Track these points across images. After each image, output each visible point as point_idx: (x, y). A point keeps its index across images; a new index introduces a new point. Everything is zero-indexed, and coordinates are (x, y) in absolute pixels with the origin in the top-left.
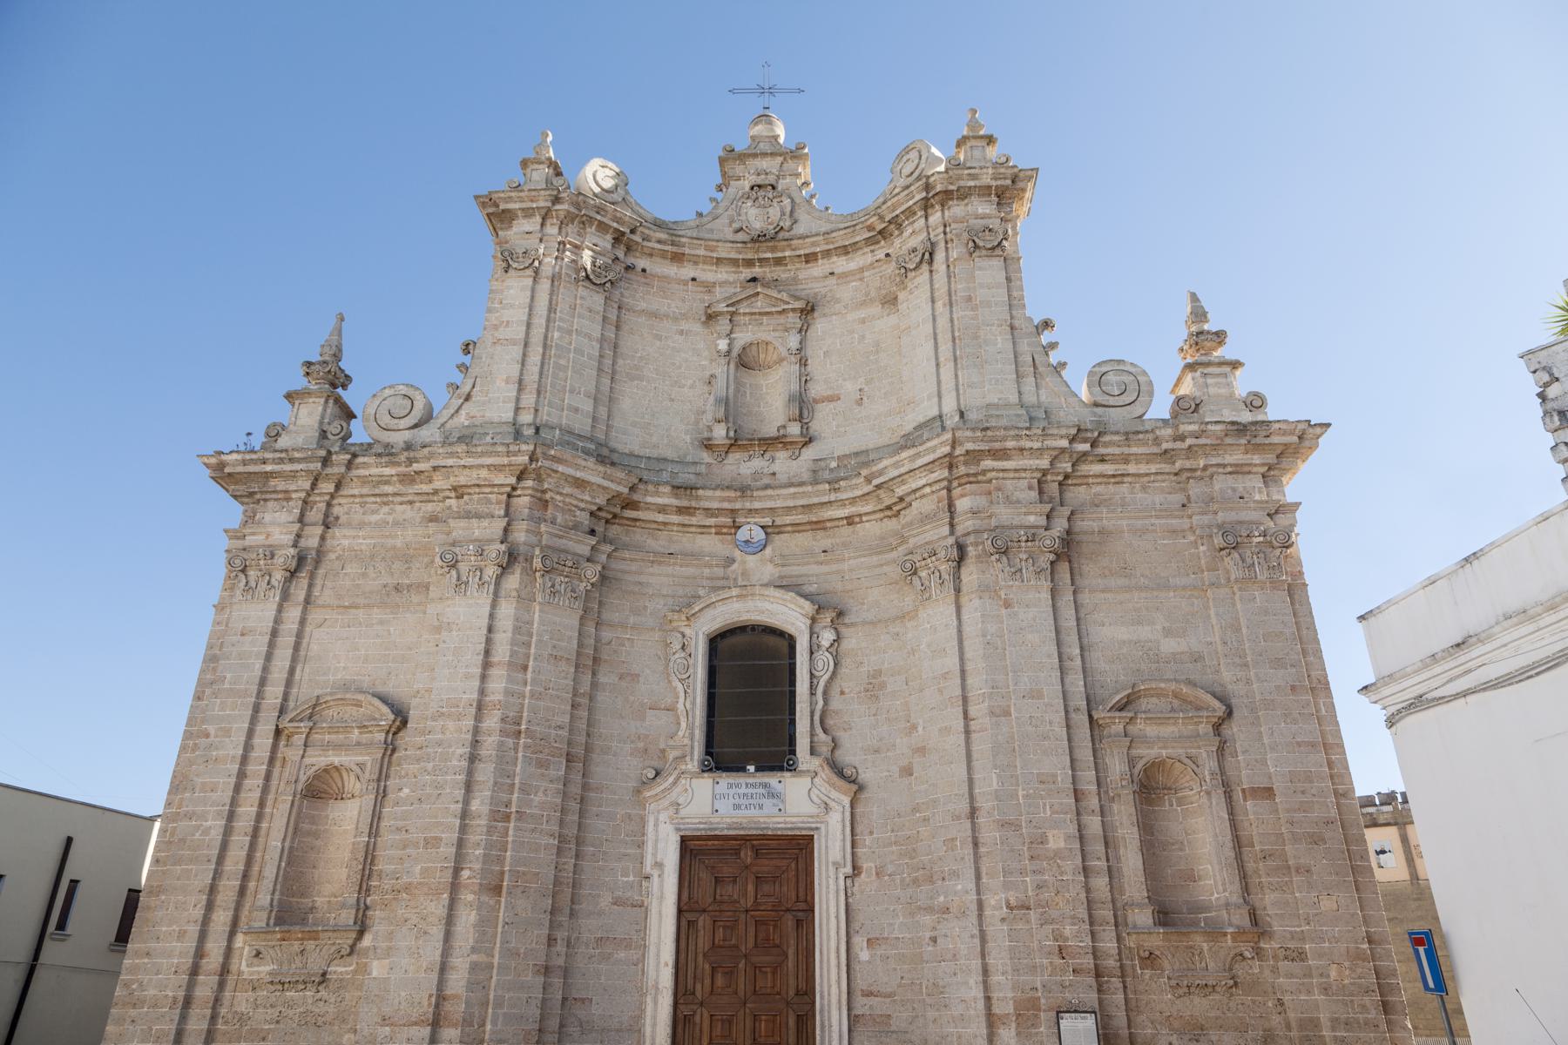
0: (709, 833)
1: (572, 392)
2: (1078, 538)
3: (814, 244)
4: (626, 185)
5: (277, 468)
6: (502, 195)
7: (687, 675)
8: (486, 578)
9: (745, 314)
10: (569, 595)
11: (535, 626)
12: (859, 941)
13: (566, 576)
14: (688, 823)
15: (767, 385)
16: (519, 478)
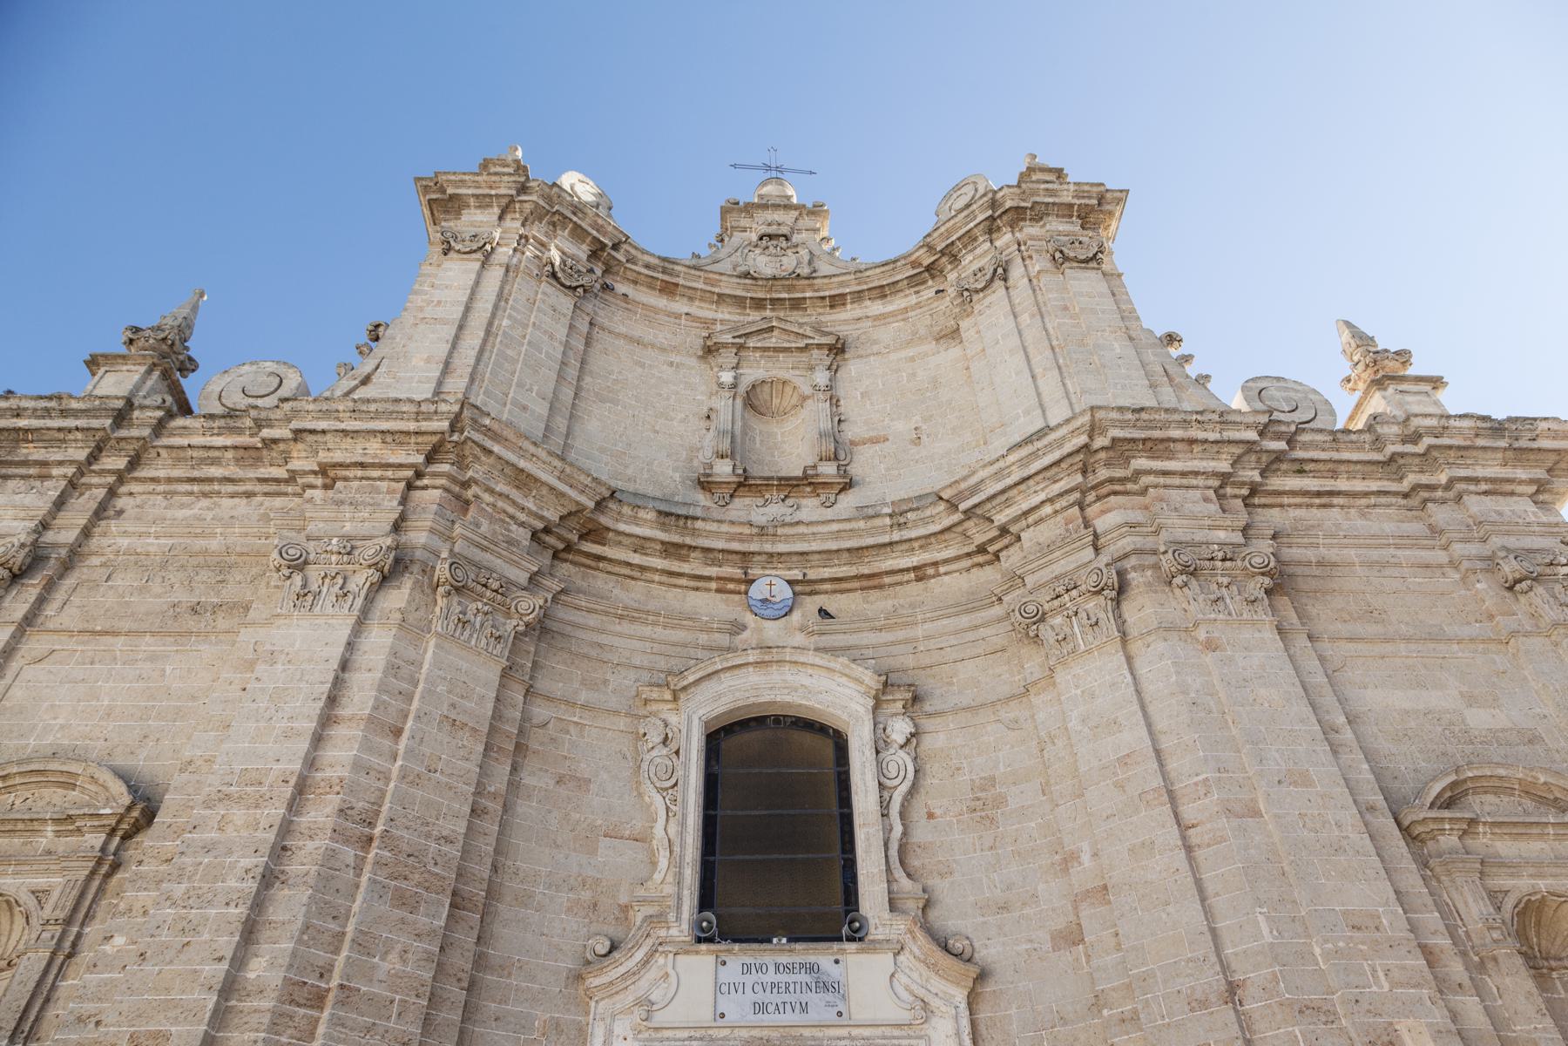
1: (520, 385)
2: (1290, 570)
3: (842, 284)
4: (610, 209)
5: (35, 423)
6: (453, 178)
7: (673, 781)
8: (351, 586)
9: (755, 348)
11: (426, 666)
15: (782, 434)
16: (430, 459)
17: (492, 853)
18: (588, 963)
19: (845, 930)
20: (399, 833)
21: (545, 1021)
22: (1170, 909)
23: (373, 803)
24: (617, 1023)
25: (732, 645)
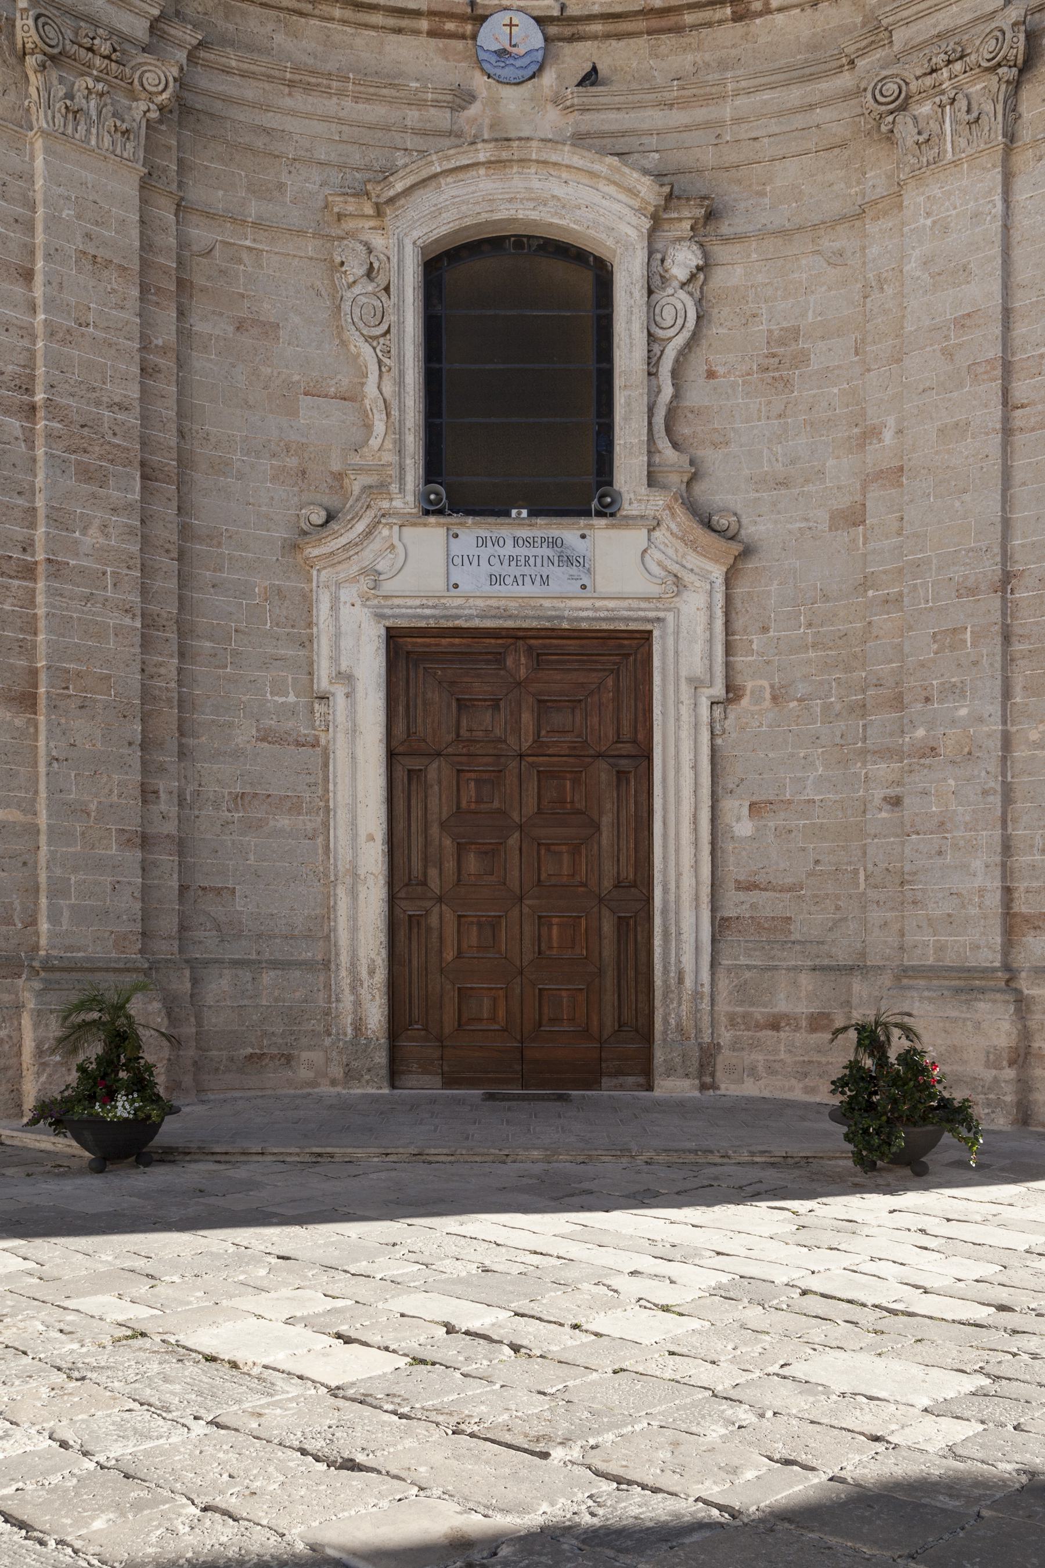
0: (444, 624)
7: (384, 327)
10: (110, 123)
11: (39, 183)
12: (735, 808)
13: (98, 80)
14: (398, 606)
17: (175, 418)
18: (305, 533)
19: (594, 504)
20: (64, 401)
21: (266, 588)
22: (966, 497)
23: (24, 366)
24: (342, 591)
25: (455, 127)
